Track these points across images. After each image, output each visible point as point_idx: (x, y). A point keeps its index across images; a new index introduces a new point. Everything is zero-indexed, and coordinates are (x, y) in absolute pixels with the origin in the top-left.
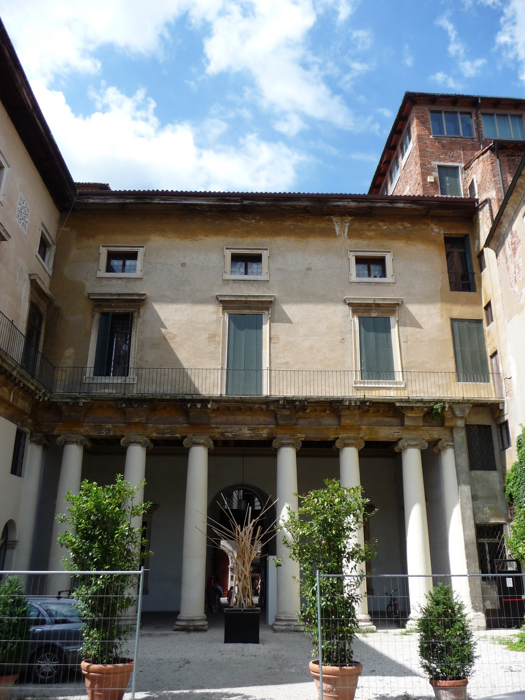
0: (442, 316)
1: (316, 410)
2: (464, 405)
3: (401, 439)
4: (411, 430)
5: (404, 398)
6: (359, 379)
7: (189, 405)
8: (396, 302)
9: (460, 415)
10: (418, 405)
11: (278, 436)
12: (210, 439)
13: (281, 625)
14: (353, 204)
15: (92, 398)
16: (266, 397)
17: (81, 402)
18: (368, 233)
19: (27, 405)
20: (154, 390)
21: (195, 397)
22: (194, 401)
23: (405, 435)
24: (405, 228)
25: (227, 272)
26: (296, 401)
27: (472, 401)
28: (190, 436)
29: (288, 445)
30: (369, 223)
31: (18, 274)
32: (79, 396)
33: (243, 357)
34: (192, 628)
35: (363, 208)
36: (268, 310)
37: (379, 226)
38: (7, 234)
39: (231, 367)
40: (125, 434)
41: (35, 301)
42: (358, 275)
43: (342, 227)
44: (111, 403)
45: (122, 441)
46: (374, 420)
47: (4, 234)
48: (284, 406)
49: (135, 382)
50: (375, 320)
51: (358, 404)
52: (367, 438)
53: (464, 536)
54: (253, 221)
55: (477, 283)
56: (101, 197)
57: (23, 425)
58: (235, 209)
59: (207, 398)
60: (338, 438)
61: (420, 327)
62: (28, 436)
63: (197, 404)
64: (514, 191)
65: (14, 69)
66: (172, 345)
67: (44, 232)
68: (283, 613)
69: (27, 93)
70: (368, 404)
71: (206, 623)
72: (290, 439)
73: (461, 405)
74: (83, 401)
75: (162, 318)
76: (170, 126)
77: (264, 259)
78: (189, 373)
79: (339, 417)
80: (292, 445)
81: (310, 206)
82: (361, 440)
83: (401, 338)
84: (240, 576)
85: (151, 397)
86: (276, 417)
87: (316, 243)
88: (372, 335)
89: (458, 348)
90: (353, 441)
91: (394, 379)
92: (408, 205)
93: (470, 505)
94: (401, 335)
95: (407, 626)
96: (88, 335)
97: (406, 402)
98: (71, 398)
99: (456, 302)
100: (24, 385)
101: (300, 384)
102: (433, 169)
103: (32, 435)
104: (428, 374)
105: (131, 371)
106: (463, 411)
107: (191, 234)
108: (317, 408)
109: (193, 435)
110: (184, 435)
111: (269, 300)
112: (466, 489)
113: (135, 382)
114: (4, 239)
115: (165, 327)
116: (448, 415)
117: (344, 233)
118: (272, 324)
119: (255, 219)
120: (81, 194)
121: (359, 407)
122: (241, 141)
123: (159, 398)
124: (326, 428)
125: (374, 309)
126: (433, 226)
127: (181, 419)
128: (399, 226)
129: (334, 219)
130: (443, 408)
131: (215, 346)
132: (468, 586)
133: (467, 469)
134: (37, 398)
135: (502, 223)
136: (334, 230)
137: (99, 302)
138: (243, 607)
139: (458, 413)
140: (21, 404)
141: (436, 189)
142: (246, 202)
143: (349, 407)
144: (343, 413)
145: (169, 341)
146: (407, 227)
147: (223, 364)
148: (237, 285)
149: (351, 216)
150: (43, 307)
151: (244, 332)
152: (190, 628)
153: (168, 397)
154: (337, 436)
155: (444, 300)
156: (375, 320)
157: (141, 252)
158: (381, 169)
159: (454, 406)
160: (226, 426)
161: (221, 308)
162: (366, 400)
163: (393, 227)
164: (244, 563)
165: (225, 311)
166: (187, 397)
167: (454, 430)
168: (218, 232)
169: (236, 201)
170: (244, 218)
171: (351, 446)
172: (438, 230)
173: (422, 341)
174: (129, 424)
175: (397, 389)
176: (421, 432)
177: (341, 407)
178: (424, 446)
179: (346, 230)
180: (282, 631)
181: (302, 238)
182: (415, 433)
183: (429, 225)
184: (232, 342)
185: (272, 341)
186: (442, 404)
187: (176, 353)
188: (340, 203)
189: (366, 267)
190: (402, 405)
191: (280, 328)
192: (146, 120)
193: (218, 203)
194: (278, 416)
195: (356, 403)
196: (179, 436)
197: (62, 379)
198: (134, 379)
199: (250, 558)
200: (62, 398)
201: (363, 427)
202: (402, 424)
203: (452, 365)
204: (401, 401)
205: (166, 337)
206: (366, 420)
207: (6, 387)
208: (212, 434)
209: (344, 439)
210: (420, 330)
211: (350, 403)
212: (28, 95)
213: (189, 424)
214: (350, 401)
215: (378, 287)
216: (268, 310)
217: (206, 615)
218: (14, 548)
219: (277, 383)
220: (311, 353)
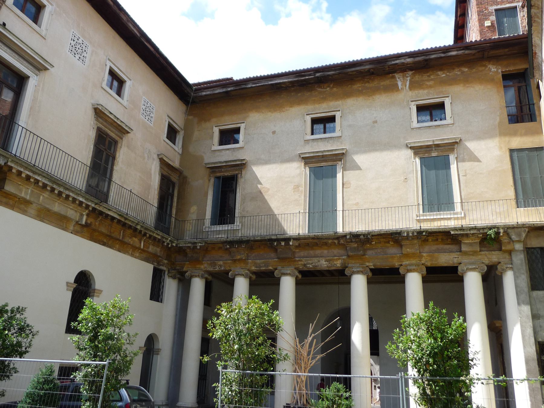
0: (501, 148)
2: (519, 229)
5: (457, 226)
6: (421, 212)
7: (275, 244)
8: (454, 141)
9: (517, 239)
10: (472, 232)
11: (350, 265)
14: (409, 60)
15: (206, 243)
18: (428, 83)
19: (158, 250)
20: (254, 233)
22: (278, 240)
23: (465, 260)
24: (463, 72)
25: (308, 133)
27: (527, 225)
28: (279, 268)
29: (358, 272)
31: (146, 155)
33: (321, 201)
35: (419, 62)
36: (341, 161)
37: (438, 75)
38: (129, 128)
39: (312, 211)
41: (165, 173)
42: (418, 122)
44: (221, 245)
46: (434, 247)
47: (126, 129)
50: (435, 160)
52: (429, 264)
54: (328, 89)
55: (537, 113)
56: (210, 90)
57: (158, 263)
58: (312, 81)
61: (479, 161)
62: (166, 273)
64: (532, 22)
65: (118, 11)
66: (266, 197)
67: (171, 122)
69: (133, 26)
70: (424, 234)
72: (358, 267)
73: (516, 230)
75: (259, 177)
76: (341, 19)
77: (338, 119)
78: (280, 219)
81: (372, 68)
83: (460, 173)
87: (381, 99)
88: (433, 173)
89: (518, 176)
91: (453, 209)
92: (460, 52)
93: (531, 324)
97: (460, 230)
98: (191, 243)
99: (515, 134)
100: (150, 235)
101: (370, 221)
102: (490, 14)
103: (169, 272)
104: (485, 203)
105: (237, 220)
106: (519, 235)
107: (279, 107)
108: (382, 240)
110: (275, 267)
112: (526, 309)
114: (128, 133)
115: (261, 184)
116: (505, 239)
117: (406, 86)
119: (329, 87)
120: (196, 90)
122: (402, 19)
123: (252, 239)
124: (391, 257)
125: (434, 149)
126: (490, 66)
127: (273, 255)
128: (457, 72)
129: (397, 75)
130: (497, 233)
133: (526, 290)
134: (165, 244)
135: (536, 53)
136: (397, 85)
137: (213, 169)
139: (514, 237)
140: (151, 249)
141: (494, 31)
142: (318, 75)
144: (403, 243)
145: (264, 194)
147: (305, 209)
148: (315, 143)
149: (411, 70)
150: (174, 178)
153: (259, 238)
155: (503, 133)
156: (435, 160)
157: (242, 126)
158: (458, 22)
159: (509, 231)
161: (303, 164)
163: (451, 74)
166: (273, 237)
167: (513, 254)
168: (300, 102)
169: (310, 75)
170: (321, 87)
171: (413, 272)
172: (495, 70)
173: (481, 173)
174: (235, 261)
175: (457, 219)
181: (369, 96)
182: (474, 257)
183: (487, 66)
184: (312, 190)
185: (345, 186)
186: (496, 230)
187: (269, 203)
188: (397, 62)
189: (428, 112)
190: (456, 233)
191: (351, 175)
192: (322, 18)
193: (296, 79)
195: (413, 233)
197: (189, 228)
200: (185, 244)
201: (424, 254)
203: (511, 193)
204: (455, 229)
205: (262, 191)
206: (427, 248)
207: (136, 237)
208: (297, 266)
210: (478, 163)
212: (134, 27)
215: (438, 130)
216: (341, 161)
218: (158, 354)
220: (380, 193)
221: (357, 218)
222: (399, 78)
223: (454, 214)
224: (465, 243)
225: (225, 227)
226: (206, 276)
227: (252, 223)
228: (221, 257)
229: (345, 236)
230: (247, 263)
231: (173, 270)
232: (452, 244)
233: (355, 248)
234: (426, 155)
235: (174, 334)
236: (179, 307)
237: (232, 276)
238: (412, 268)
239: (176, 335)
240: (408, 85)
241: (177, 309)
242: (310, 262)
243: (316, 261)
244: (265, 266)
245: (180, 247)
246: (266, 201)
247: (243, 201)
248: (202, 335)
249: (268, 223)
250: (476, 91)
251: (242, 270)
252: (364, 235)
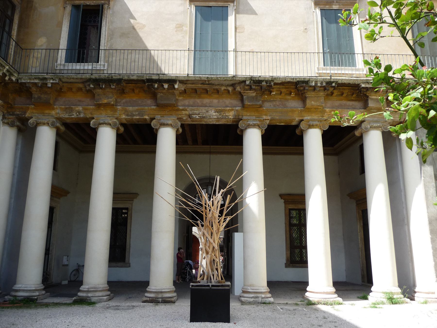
1: (281, 93)
7: (156, 86)
11: (244, 118)
12: (177, 121)
13: (247, 298)
15: (60, 80)
16: (232, 77)
17: (50, 83)
21: (162, 77)
22: (161, 82)
26: (262, 81)
28: (158, 117)
29: (254, 126)
32: (47, 77)
34: (160, 299)
39: (198, 49)
40: (95, 116)
44: (81, 86)
45: (91, 122)
46: (337, 103)
48: (251, 86)
49: (106, 68)
51: (324, 84)
53: (428, 212)
59: (174, 78)
60: (302, 120)
63: (164, 84)
66: (141, 34)
68: (250, 286)
70: (334, 84)
71: (175, 294)
72: (254, 120)
74: (51, 81)
75: (132, 8)
79: (304, 100)
80: (259, 127)
84: (207, 248)
85: (118, 77)
86: (242, 100)
90: (317, 123)
95: (369, 297)
96: (60, 25)
98: (39, 79)
109: (161, 117)
112: (429, 170)
113: (106, 68)
115: (134, 18)
118: (237, 15)
121: (325, 88)
123: (126, 78)
124: (287, 111)
131: (182, 35)
132: (433, 261)
138: (211, 282)
145: (138, 31)
151: (210, 23)
152: (159, 300)
154: (301, 118)
160: (193, 108)
162: (332, 80)
164: (212, 233)
165: (192, 3)
166: (154, 77)
171: (315, 128)
174: (99, 106)
177: (307, 88)
180: (250, 303)
184: (198, 32)
185: (237, 31)
191: (243, 19)
194: (244, 97)
195: (322, 83)
197: (35, 64)
198: (104, 65)
199: (218, 229)
200: (30, 79)
205: (136, 27)
206: (329, 103)
208: (180, 116)
209: (308, 121)
211: (316, 84)
213: (157, 106)
214: (316, 82)
217: (175, 287)
219: (242, 65)
221: (252, 66)
223: (357, 70)
224: (372, 99)
225: (88, 66)
226: (58, 125)
227: (121, 63)
228: (80, 101)
229: (244, 82)
230: (116, 111)
231: (10, 115)
233: (253, 97)
235: (11, 198)
236: (17, 165)
237: (95, 125)
238: (315, 123)
239: (13, 200)
241: (14, 167)
242: (197, 112)
243: (204, 111)
244: (139, 115)
245: (21, 83)
246: (141, 39)
247: (111, 36)
248: (50, 204)
249: (144, 65)
251: (108, 118)
252: (267, 82)
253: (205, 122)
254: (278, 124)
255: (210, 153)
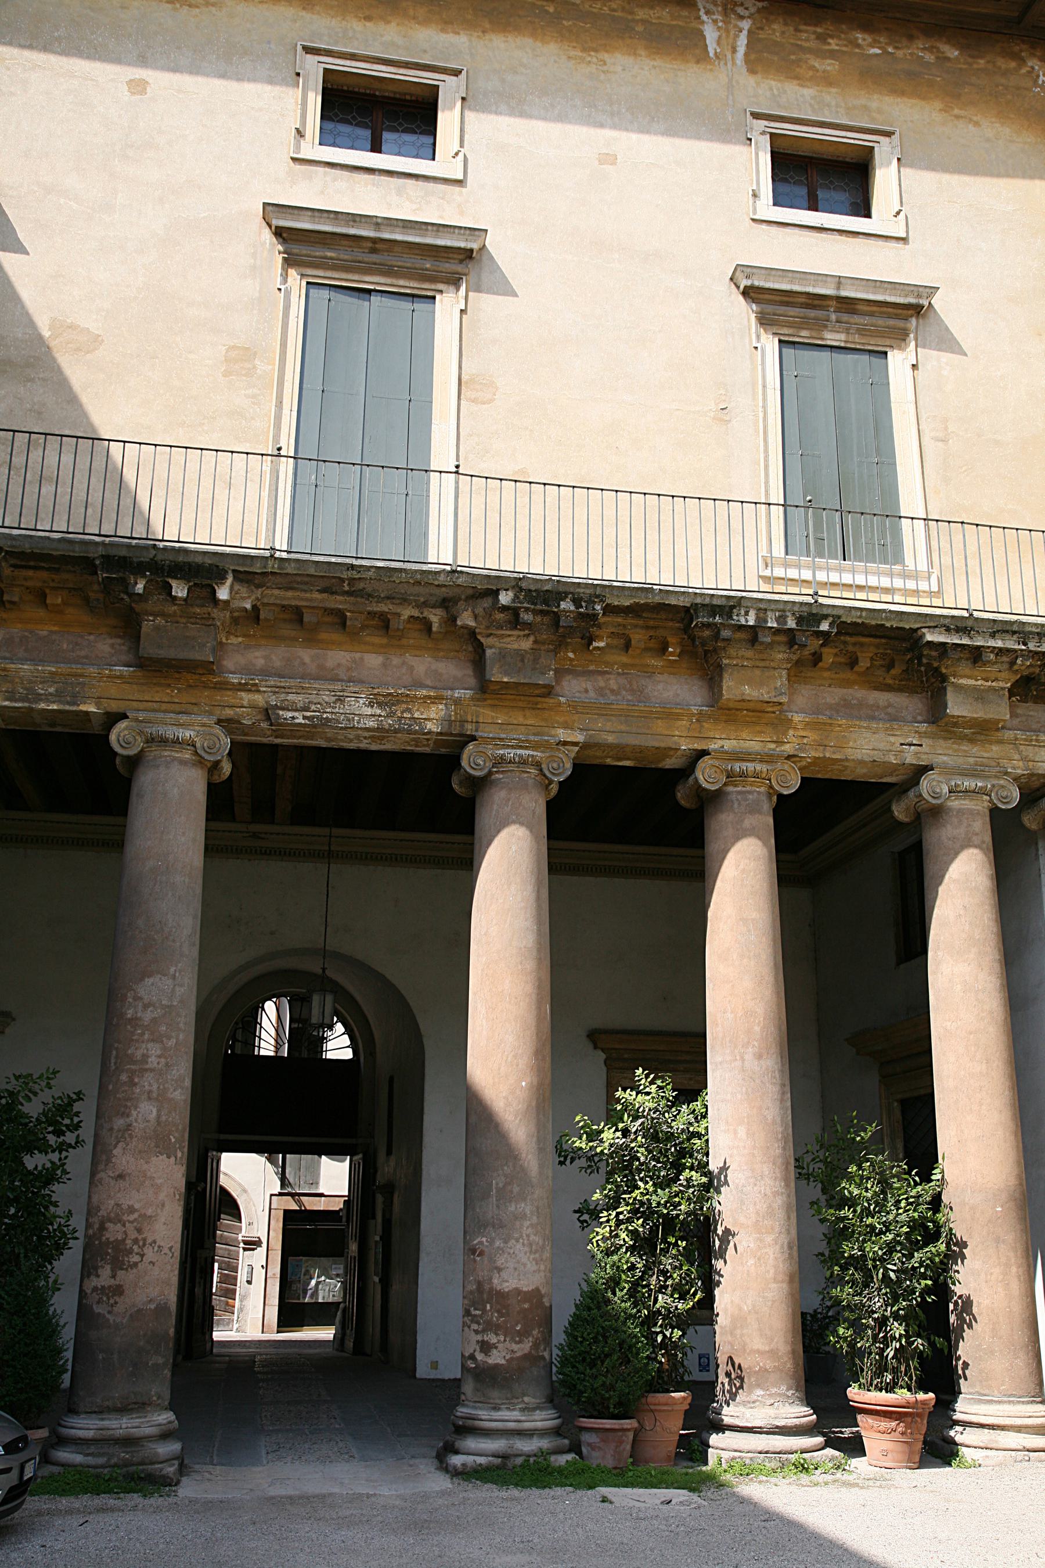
3: (926, 769)
4: (963, 738)
6: (778, 550)
7: (140, 587)
8: (912, 300)
10: (999, 644)
12: (218, 730)
24: (944, 59)
30: (819, 30)
33: (359, 426)
43: (728, 31)
46: (833, 695)
60: (704, 753)
63: (174, 583)
82: (787, 766)
86: (479, 662)
94: (923, 416)
110: (114, 707)
111: (462, 245)
117: (734, 50)
121: (790, 638)
124: (658, 713)
127: (105, 646)
143: (753, 634)
146: (948, 59)
163: (900, 54)
176: (994, 748)
177: (726, 633)
178: (1003, 799)
179: (742, 41)
182: (975, 750)
183: (1022, 61)
184: (315, 383)
194: (489, 652)
196: (92, 709)
201: (797, 718)
202: (936, 714)
206: (805, 695)
208: (229, 712)
211: (761, 620)
214: (763, 607)
222: (707, 13)
223: (905, 575)
224: (959, 688)
232: (900, 690)
233: (521, 655)
234: (804, 335)
240: (741, 50)
242: (299, 699)
244: (58, 696)
250: (988, 140)
253: (329, 740)
254: (609, 761)
255: (329, 856)
